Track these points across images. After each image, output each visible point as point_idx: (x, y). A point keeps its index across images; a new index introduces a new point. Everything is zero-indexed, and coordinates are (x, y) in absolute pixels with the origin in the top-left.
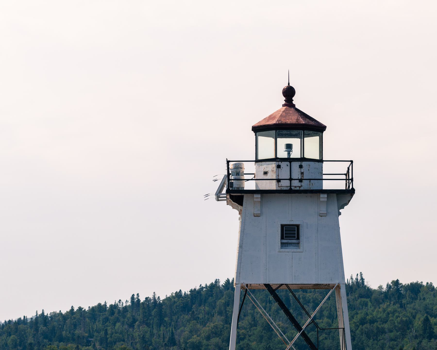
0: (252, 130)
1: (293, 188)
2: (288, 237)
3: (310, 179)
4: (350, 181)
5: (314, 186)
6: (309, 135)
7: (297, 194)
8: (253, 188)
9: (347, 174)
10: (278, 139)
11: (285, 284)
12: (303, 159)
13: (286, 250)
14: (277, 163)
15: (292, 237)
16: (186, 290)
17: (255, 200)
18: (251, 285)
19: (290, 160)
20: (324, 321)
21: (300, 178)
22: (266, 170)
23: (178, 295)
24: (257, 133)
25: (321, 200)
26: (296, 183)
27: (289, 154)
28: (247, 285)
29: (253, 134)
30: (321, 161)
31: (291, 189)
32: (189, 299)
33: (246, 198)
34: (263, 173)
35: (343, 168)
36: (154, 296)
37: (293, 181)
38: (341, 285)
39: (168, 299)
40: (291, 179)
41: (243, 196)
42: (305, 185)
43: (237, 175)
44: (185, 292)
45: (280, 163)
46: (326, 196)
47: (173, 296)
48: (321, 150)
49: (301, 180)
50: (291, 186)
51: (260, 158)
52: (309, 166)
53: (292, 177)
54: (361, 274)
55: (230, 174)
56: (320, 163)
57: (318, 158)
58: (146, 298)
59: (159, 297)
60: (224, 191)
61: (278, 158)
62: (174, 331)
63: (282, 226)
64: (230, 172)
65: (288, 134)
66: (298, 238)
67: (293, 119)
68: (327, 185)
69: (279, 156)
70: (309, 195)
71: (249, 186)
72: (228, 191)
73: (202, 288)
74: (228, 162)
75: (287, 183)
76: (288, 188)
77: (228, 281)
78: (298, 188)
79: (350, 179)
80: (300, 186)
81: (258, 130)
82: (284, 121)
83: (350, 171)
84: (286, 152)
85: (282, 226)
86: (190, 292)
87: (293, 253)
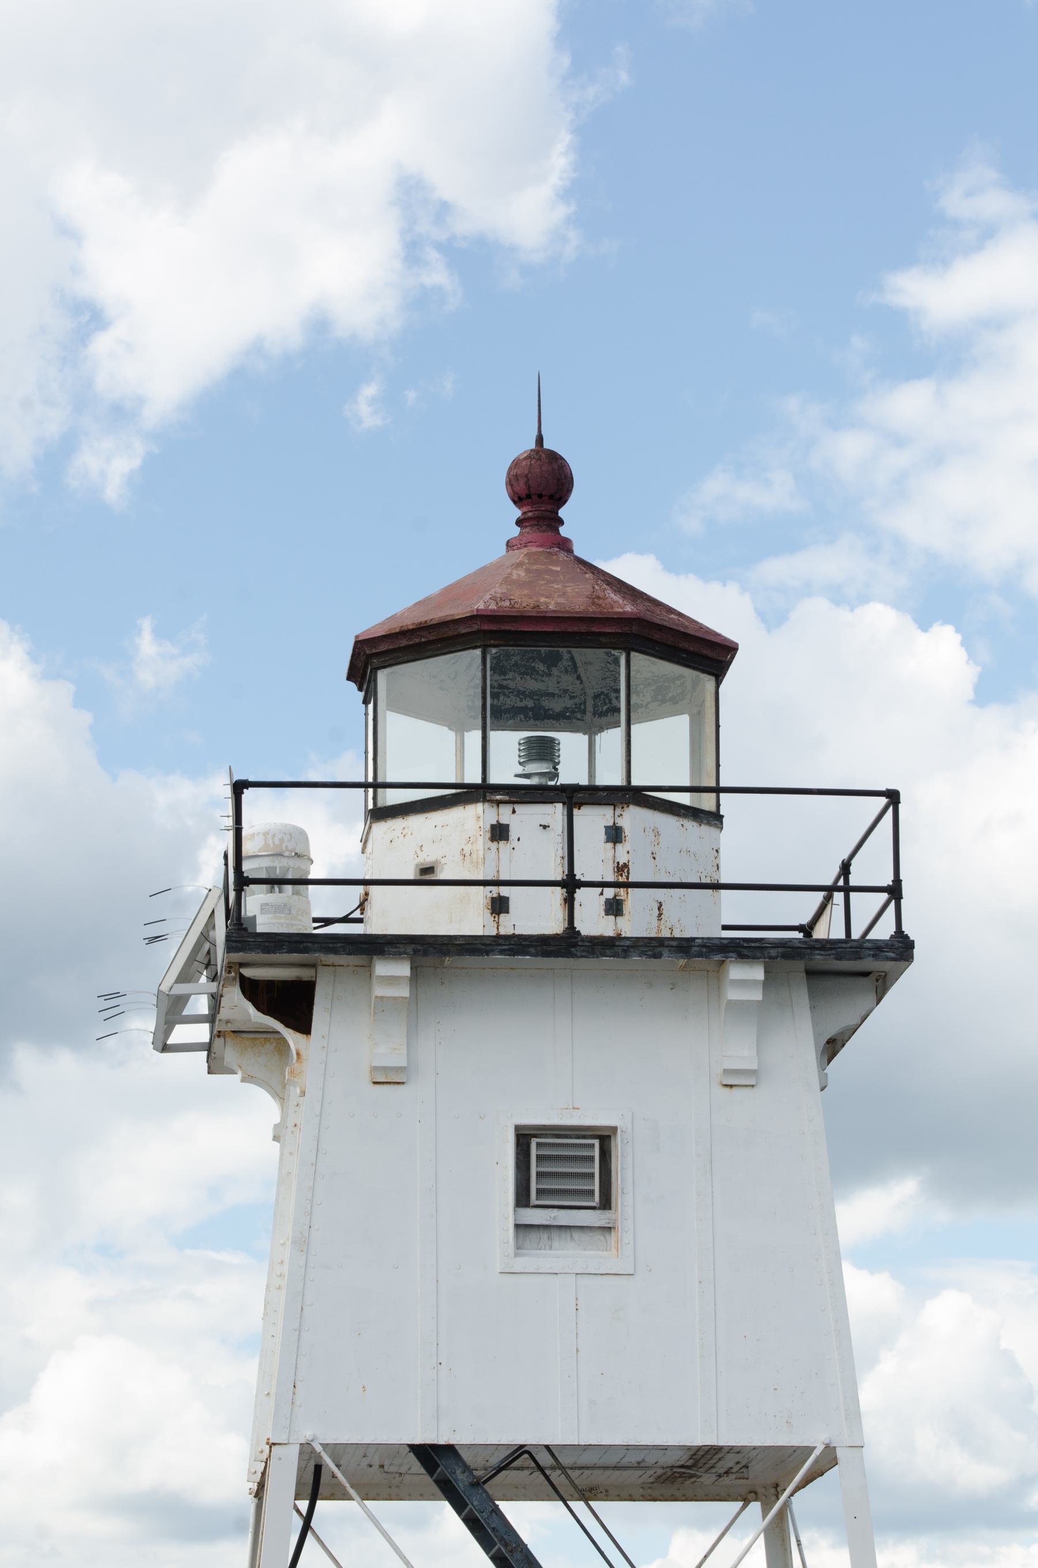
8: (464, 916)
22: (277, 1285)
25: (733, 994)
42: (638, 920)
45: (504, 814)
52: (657, 834)
53: (580, 874)
56: (705, 830)
66: (606, 1203)
67: (563, 596)
82: (523, 600)
85: (524, 1137)
87: (584, 1281)
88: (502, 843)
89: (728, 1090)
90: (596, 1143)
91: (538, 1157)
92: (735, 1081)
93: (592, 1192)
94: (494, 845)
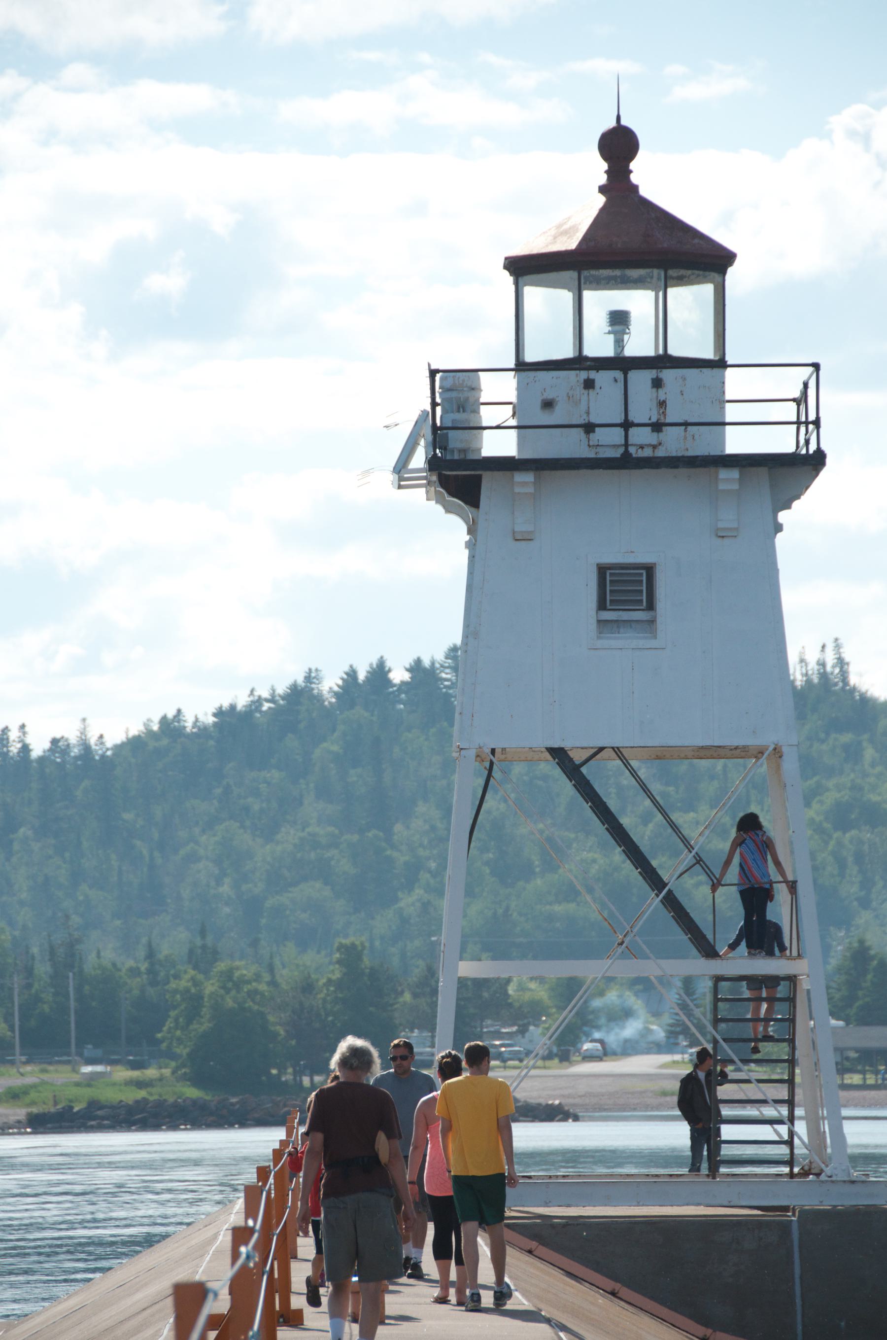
0: (506, 267)
1: (632, 450)
2: (620, 604)
3: (686, 424)
4: (811, 427)
5: (700, 447)
6: (681, 281)
7: (646, 470)
9: (801, 401)
10: (587, 294)
11: (613, 748)
12: (664, 361)
13: (613, 643)
14: (584, 375)
15: (631, 604)
16: (199, 710)
17: (517, 490)
18: (504, 749)
19: (622, 364)
20: (806, 971)
21: (654, 420)
22: (549, 395)
23: (170, 727)
24: (520, 279)
25: (722, 486)
26: (641, 436)
27: (619, 343)
28: (493, 751)
29: (508, 280)
30: (721, 364)
31: (626, 454)
32: (212, 743)
33: (489, 483)
34: (539, 404)
35: (790, 383)
36: (83, 732)
37: (633, 431)
38: (785, 749)
39: (135, 745)
40: (627, 425)
41: (479, 479)
42: (673, 443)
43: (459, 411)
44: (197, 720)
45: (593, 374)
46: (734, 474)
47: (150, 733)
48: (721, 329)
49: (657, 427)
50: (626, 445)
51: (530, 357)
52: (685, 379)
54: (838, 646)
55: (438, 405)
56: (716, 371)
57: (708, 353)
58: (55, 742)
59: (101, 737)
60: (419, 460)
61: (587, 358)
62: (159, 861)
63: (602, 570)
64: (438, 400)
65: (614, 278)
66: (651, 606)
68: (738, 442)
69: (590, 351)
70: (683, 471)
71: (499, 444)
72: (433, 463)
73: (259, 701)
74: (433, 373)
75: (615, 436)
76: (617, 453)
77: (352, 674)
78: (647, 453)
79: (813, 423)
80: (655, 442)
81: (525, 268)
83: (812, 392)
84: (612, 336)
85: (602, 570)
86: (215, 715)
88: (591, 391)
89: (720, 539)
90: (644, 572)
91: (610, 581)
92: (721, 535)
93: (641, 601)
94: (586, 392)
